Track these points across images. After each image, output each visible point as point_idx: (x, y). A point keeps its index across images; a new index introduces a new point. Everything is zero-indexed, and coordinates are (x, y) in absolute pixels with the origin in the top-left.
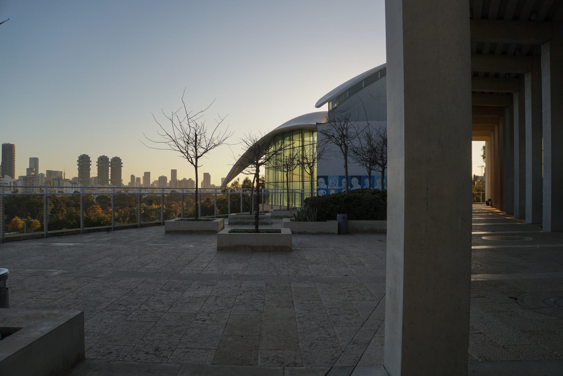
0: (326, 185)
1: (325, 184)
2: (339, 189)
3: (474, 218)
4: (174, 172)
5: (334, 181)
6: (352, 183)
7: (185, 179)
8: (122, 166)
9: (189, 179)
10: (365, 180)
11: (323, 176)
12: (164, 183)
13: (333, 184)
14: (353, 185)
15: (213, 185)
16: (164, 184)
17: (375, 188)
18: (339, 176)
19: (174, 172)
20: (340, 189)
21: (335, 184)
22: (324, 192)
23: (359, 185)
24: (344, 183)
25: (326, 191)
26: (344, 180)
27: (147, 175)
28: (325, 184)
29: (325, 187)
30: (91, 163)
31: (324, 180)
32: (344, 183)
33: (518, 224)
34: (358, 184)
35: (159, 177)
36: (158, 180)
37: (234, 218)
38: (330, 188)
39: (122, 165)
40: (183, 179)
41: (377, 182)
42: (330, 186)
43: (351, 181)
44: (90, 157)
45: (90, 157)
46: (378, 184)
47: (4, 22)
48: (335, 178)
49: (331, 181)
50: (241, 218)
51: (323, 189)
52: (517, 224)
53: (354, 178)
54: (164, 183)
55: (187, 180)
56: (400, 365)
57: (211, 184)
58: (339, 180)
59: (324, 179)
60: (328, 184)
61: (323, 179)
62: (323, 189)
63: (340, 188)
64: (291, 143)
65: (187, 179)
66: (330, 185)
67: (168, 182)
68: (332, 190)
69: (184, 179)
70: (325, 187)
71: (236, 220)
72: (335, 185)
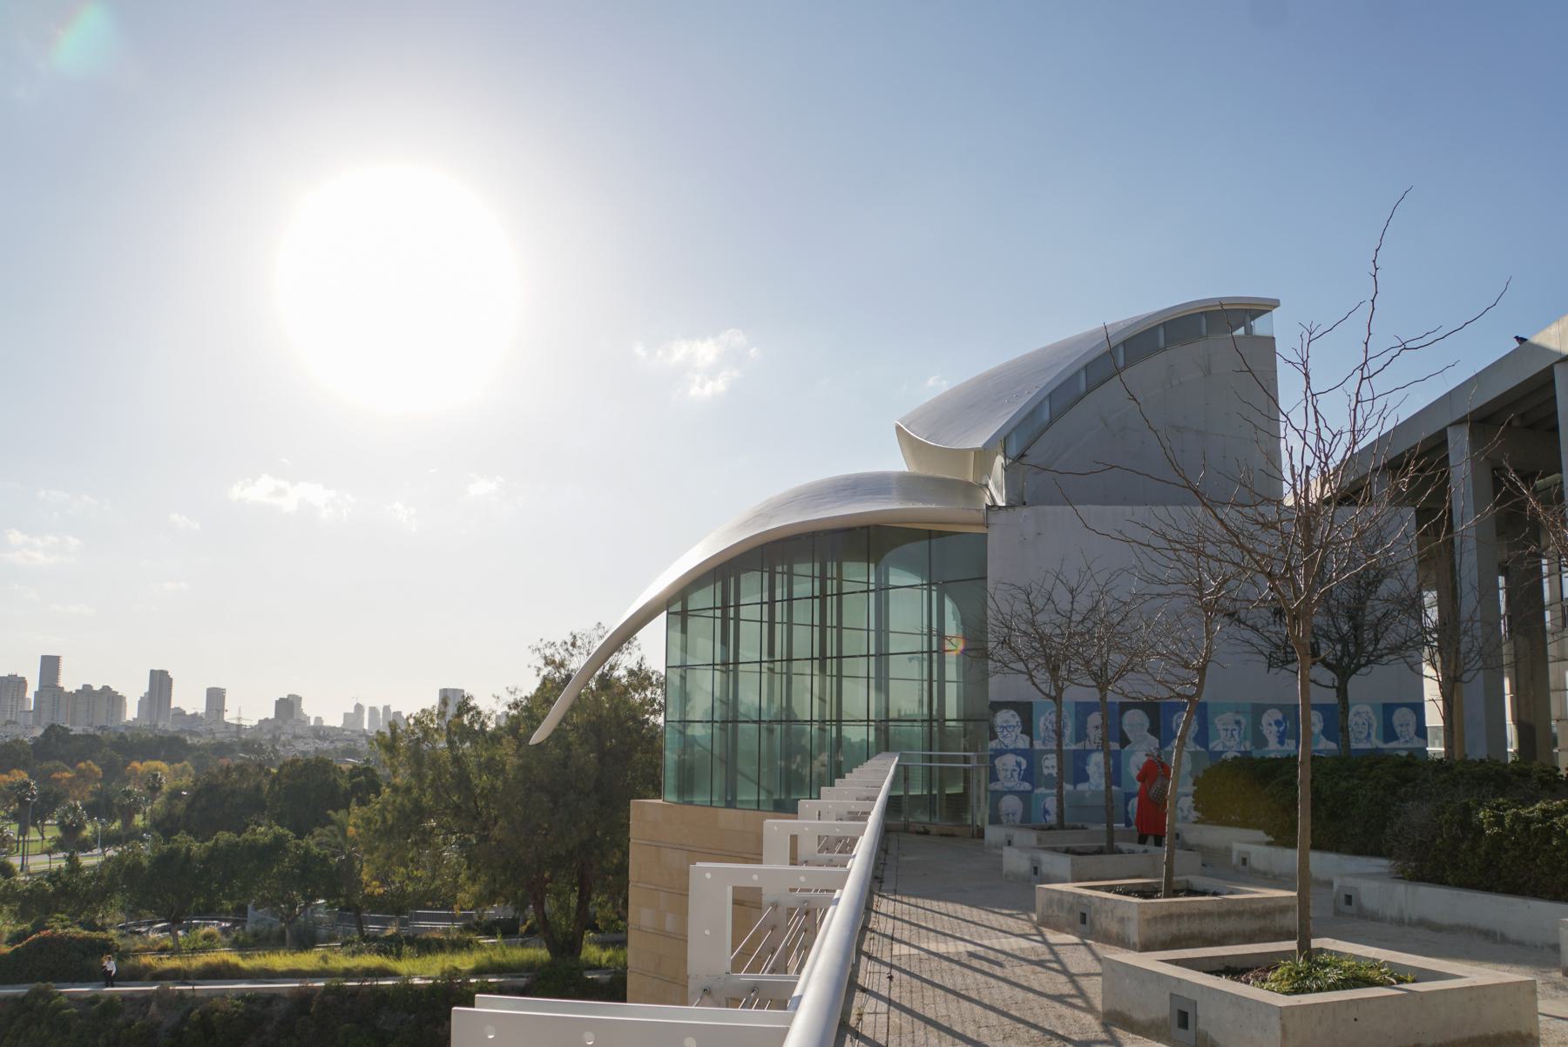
0: (1024, 736)
1: (1022, 733)
2: (1075, 751)
4: (50, 666)
6: (1126, 729)
7: (87, 688)
9: (101, 687)
10: (1175, 717)
11: (1015, 703)
12: (15, 700)
14: (1131, 736)
15: (179, 708)
16: (14, 703)
17: (1211, 746)
18: (1077, 704)
19: (50, 666)
20: (1081, 750)
22: (1019, 764)
23: (1153, 737)
24: (1097, 727)
25: (1024, 757)
26: (1095, 719)
27: (161, 683)
28: (1022, 733)
29: (1023, 743)
32: (1097, 727)
34: (1148, 731)
36: (352, 711)
37: (1163, 918)
38: (1043, 747)
40: (81, 688)
41: (1220, 726)
42: (1040, 742)
43: (1121, 723)
46: (1223, 733)
49: (1046, 719)
50: (1191, 916)
51: (1015, 752)
53: (1132, 711)
54: (15, 700)
55: (96, 692)
58: (1077, 718)
59: (1019, 715)
60: (1034, 732)
61: (1012, 712)
62: (1015, 752)
63: (1080, 746)
64: (1042, 590)
65: (97, 687)
66: (1042, 735)
68: (1049, 756)
69: (84, 686)
70: (1023, 743)
71: (1173, 928)
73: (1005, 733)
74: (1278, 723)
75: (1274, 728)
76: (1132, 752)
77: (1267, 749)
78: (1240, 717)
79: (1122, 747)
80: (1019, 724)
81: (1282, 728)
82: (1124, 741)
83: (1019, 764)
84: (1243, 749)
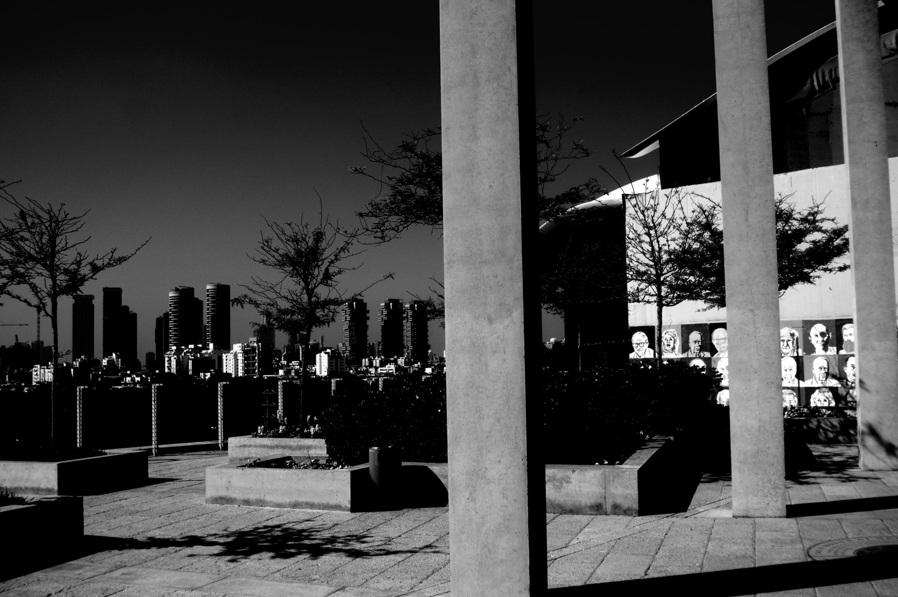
1: (649, 347)
3: (169, 368)
5: (671, 340)
8: (368, 318)
13: (669, 345)
18: (682, 326)
21: (672, 346)
28: (649, 347)
30: (368, 315)
31: (646, 338)
33: (303, 549)
35: (93, 295)
39: (368, 315)
44: (366, 304)
45: (366, 304)
47: (75, 245)
48: (671, 330)
52: (292, 541)
56: (845, 271)
57: (123, 304)
58: (682, 336)
61: (643, 334)
63: (685, 355)
67: (287, 550)
72: (673, 349)
73: (639, 347)
74: (822, 334)
75: (820, 338)
76: (719, 359)
77: (814, 354)
78: (793, 331)
79: (712, 355)
80: (647, 341)
81: (825, 339)
82: (714, 351)
83: (792, 335)
84: (795, 354)
